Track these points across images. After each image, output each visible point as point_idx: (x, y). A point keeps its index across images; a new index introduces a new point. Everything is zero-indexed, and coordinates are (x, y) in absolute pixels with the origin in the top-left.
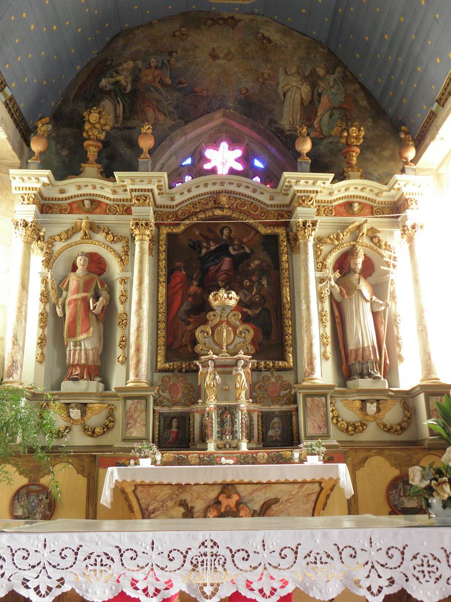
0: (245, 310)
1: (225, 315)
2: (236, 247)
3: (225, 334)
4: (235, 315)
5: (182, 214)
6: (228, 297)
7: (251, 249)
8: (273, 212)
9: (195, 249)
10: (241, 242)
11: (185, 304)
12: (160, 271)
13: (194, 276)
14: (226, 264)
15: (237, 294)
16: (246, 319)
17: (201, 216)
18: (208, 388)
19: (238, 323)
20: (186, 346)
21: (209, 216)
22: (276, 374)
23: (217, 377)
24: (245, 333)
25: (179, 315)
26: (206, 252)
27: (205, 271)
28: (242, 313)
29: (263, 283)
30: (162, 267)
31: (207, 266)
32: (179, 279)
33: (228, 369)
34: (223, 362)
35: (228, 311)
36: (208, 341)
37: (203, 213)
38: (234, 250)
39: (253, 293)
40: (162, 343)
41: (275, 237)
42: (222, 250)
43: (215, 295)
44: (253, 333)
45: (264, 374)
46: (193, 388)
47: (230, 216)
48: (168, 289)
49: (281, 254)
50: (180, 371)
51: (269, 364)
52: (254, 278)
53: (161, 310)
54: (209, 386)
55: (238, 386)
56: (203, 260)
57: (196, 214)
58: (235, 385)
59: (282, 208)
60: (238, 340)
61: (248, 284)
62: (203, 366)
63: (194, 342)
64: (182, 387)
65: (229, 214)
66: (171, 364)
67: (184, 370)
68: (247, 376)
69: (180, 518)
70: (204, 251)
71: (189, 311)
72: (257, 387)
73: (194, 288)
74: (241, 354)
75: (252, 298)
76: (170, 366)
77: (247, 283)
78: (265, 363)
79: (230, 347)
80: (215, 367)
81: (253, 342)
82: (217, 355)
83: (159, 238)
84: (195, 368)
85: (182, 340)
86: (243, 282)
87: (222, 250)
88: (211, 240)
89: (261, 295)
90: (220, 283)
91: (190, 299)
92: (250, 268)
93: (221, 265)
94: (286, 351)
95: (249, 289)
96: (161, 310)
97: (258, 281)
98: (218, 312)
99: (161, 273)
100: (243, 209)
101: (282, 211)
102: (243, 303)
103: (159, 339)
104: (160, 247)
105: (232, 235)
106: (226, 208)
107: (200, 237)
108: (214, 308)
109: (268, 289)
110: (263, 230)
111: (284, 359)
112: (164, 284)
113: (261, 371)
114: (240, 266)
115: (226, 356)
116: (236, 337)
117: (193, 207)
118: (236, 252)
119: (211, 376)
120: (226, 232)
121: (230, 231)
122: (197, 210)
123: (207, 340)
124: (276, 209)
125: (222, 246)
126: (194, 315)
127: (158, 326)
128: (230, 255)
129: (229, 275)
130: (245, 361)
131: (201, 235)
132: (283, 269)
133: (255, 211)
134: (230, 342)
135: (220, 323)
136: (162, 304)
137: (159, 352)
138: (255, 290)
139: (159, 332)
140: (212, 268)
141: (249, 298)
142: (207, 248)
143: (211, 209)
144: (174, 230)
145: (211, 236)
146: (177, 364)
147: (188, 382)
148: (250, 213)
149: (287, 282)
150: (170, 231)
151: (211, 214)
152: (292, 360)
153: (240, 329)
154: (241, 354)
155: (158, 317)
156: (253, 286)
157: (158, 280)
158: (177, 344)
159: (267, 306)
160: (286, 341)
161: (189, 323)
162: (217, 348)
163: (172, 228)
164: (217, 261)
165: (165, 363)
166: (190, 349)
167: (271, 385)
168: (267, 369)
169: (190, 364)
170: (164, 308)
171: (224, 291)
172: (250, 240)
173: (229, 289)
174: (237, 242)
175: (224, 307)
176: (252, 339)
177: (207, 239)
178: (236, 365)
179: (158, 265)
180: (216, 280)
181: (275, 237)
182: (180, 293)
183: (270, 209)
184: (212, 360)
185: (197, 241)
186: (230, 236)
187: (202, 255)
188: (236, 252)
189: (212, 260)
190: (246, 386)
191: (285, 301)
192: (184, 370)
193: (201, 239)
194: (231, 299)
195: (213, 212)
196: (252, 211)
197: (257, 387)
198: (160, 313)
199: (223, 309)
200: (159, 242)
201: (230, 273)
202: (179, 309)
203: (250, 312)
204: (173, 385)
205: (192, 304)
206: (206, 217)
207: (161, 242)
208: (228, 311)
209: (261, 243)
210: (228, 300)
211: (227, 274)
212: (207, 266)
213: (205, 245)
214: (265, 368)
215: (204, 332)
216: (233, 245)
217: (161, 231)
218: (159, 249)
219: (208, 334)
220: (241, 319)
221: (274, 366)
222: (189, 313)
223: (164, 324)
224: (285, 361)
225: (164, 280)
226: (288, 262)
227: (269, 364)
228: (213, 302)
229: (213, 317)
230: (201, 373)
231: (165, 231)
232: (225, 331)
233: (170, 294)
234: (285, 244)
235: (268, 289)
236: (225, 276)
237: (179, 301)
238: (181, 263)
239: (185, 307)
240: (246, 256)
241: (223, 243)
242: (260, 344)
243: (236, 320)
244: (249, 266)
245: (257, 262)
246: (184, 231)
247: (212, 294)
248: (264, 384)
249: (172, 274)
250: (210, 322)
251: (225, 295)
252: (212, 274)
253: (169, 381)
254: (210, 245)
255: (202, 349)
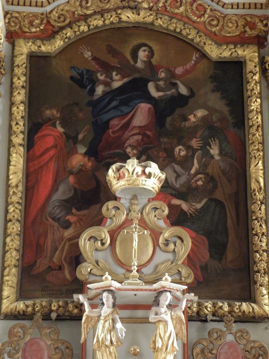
0: (176, 202)
1: (138, 208)
2: (161, 83)
3: (135, 244)
4: (156, 209)
5: (59, 18)
6: (144, 172)
7: (191, 90)
8: (232, 31)
9: (82, 85)
10: (172, 75)
11: (61, 189)
12: (13, 124)
13: (80, 137)
14: (142, 115)
15: (162, 169)
16: (177, 218)
17: (95, 23)
18: (99, 347)
19: (161, 223)
20: (60, 268)
21: (112, 23)
22: (235, 327)
23: (119, 325)
24: (175, 244)
25: (49, 209)
26: (103, 91)
27: (101, 128)
28: (170, 206)
29: (212, 152)
30: (19, 117)
31: (105, 117)
32: (50, 142)
33: (140, 313)
34: (129, 297)
35: (143, 200)
36: (104, 257)
37: (98, 17)
38: (158, 89)
39: (193, 171)
40: (14, 262)
41: (238, 65)
42: (136, 89)
43: (118, 170)
44: (190, 244)
45: (211, 326)
46: (72, 350)
47: (152, 24)
48: (29, 160)
49: (249, 97)
50: (46, 317)
51: (221, 308)
52: (195, 143)
53: (15, 199)
54: (101, 344)
55: (159, 344)
56: (98, 107)
57: (85, 18)
58: (154, 342)
59: (252, 11)
60: (161, 257)
61: (183, 153)
62: (93, 306)
63: (77, 259)
64: (49, 347)
65: (150, 19)
66: (29, 302)
67: (54, 315)
68: (178, 326)
69: (258, 3)
70: (100, 90)
71: (67, 201)
72: (198, 350)
73: (79, 159)
74: (166, 282)
75: (189, 181)
76: (27, 306)
77: (180, 151)
78: (214, 305)
79: (145, 270)
80: (114, 305)
81: (190, 261)
82: (121, 282)
83: (12, 62)
84: (76, 311)
85: (52, 257)
86: (173, 150)
87: (136, 89)
88: (113, 68)
89: (207, 174)
90: (129, 150)
91: (71, 179)
92: (187, 124)
93: (133, 116)
94: (256, 283)
95: (186, 163)
96: (15, 199)
97: (201, 148)
98: (124, 202)
99: (15, 128)
100: (176, 11)
101: (252, 16)
102: (174, 189)
103: (8, 255)
104: (15, 80)
105: (153, 61)
106: (145, 9)
107: (93, 63)
108: (118, 195)
109: (221, 164)
110: (214, 52)
111: (251, 298)
112: (21, 149)
113: (206, 321)
114: (169, 119)
115: (137, 284)
116: (158, 249)
117: (81, 5)
118: (161, 94)
119: (107, 324)
120: (142, 54)
121: (152, 53)
122: (89, 12)
123: (100, 256)
124: (241, 12)
125: (134, 81)
126: (79, 209)
127: (6, 229)
128: (149, 99)
129: (148, 137)
130: (175, 298)
131: (94, 58)
132: (251, 127)
133: (200, 17)
134: (145, 259)
135: (128, 222)
136: (17, 186)
137: (6, 278)
138: (196, 165)
139: (8, 240)
140: (114, 122)
141: (183, 179)
142: (107, 84)
143: (115, 10)
144: (43, 48)
145: (114, 62)
146: (41, 303)
147: (60, 338)
148: (189, 19)
149: (258, 150)
150: (34, 48)
151: (114, 19)
152: (267, 301)
153: (166, 235)
154: (166, 282)
155: (7, 211)
156: (193, 157)
157: (10, 141)
158: (42, 265)
159: (218, 195)
160: (255, 262)
161: (67, 225)
162: (121, 271)
163: (39, 42)
164: (125, 109)
165: (17, 300)
166: (68, 275)
167: (226, 347)
168: (218, 317)
169: (67, 304)
170: (19, 195)
171: (136, 161)
172: (187, 72)
173: (145, 155)
174: (163, 75)
175: (135, 193)
176: (189, 256)
177: (107, 68)
178: (156, 302)
179: (11, 114)
180: (121, 145)
181: (238, 65)
182: (52, 166)
183: (229, 11)
184: (110, 291)
185: (88, 71)
186: (150, 62)
187: (95, 98)
188: (161, 94)
189: (115, 108)
190: (175, 344)
191: (254, 186)
192: (54, 315)
193: (94, 66)
194: (149, 176)
195: (118, 15)
196: (195, 14)
197: (198, 350)
198: (12, 203)
199: (135, 197)
200: (13, 70)
201: (148, 133)
202: (49, 197)
203: (185, 206)
204: (32, 342)
205: (75, 190)
206: (104, 25)
207: (16, 70)
208: (143, 200)
209: (211, 77)
210: (143, 178)
211: (144, 135)
212: (105, 117)
213: (101, 78)
214: (214, 315)
215: (96, 239)
216: (156, 80)
217: (17, 48)
218: (12, 83)
219: (103, 244)
220: (168, 217)
221: (231, 312)
222: (69, 204)
223: (18, 225)
224: (255, 302)
225: (21, 142)
226: (261, 112)
227: (221, 308)
228: (114, 182)
229: (113, 212)
230: (88, 317)
231: (24, 48)
232: (136, 236)
233: (32, 170)
234: (257, 77)
235: (221, 164)
236: (139, 137)
237: (50, 182)
238: (55, 112)
239: (62, 193)
240: (180, 101)
241: (136, 75)
242: (204, 268)
243: (158, 217)
244: (186, 119)
245: (200, 113)
246: (63, 51)
247: (114, 167)
248: (211, 346)
249: (36, 132)
250: (109, 220)
251: (139, 170)
252: (113, 133)
253: (24, 334)
254: (111, 78)
255: (90, 273)
